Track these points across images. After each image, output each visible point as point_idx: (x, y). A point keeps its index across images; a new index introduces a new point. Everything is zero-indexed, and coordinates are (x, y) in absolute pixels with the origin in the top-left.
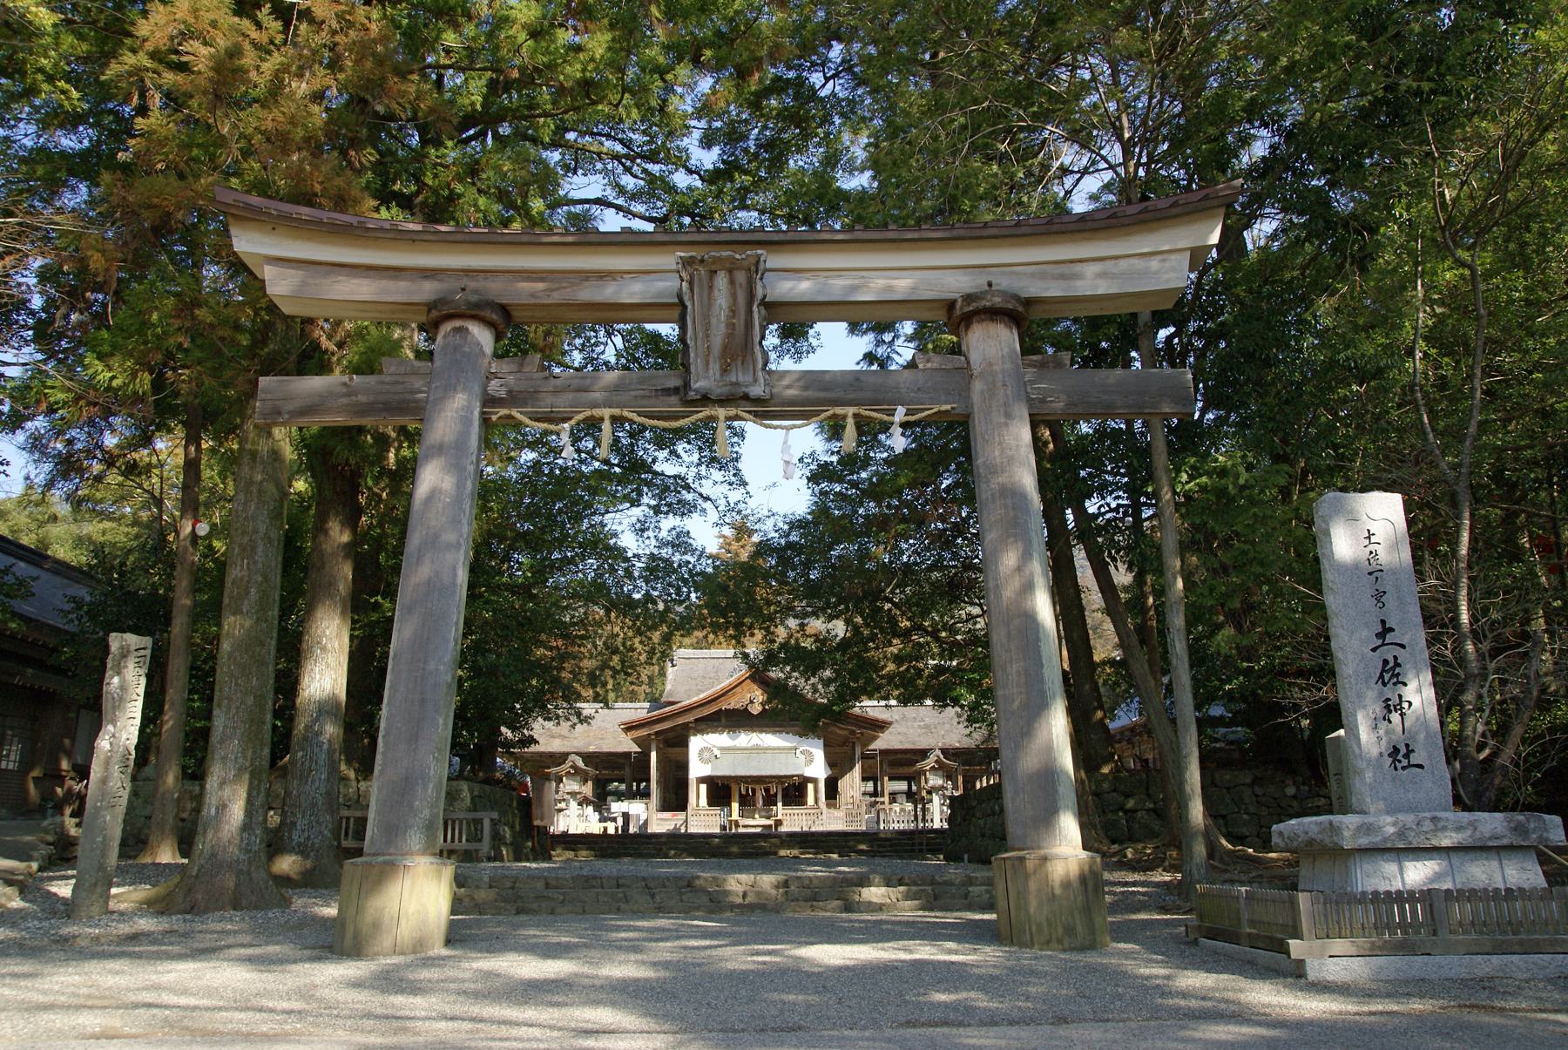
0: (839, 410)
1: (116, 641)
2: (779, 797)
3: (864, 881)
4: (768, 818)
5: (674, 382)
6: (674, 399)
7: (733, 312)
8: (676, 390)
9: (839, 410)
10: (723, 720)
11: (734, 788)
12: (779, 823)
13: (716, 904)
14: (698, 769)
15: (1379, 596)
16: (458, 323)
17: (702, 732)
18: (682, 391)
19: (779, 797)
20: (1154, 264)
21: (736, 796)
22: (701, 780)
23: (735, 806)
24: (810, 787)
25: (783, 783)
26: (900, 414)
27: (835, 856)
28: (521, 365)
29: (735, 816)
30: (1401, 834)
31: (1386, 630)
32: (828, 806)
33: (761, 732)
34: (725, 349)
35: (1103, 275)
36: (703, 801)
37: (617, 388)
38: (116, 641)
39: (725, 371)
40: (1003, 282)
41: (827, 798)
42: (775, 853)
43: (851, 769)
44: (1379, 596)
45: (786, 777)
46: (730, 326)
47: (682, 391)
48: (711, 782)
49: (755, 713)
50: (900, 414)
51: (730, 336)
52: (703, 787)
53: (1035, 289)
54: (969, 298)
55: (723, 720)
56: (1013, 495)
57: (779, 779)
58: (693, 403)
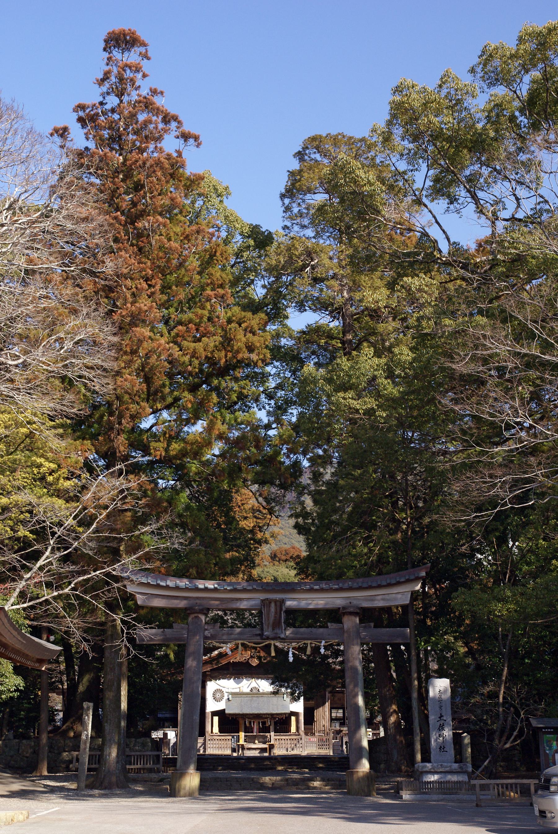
0: (306, 642)
1: (85, 705)
2: (272, 728)
3: (312, 779)
4: (264, 743)
5: (258, 632)
6: (259, 637)
7: (276, 613)
8: (259, 635)
9: (306, 642)
10: (231, 669)
11: (241, 722)
12: (272, 747)
13: (262, 787)
14: (212, 706)
15: (441, 707)
16: (196, 615)
17: (216, 678)
18: (261, 635)
19: (272, 728)
20: (399, 596)
21: (242, 727)
22: (214, 714)
23: (242, 735)
24: (293, 718)
25: (275, 718)
26: (323, 643)
27: (307, 770)
28: (214, 626)
29: (242, 742)
30: (433, 768)
31: (441, 716)
32: (306, 734)
33: (258, 678)
34: (274, 623)
35: (383, 599)
36: (216, 729)
37: (240, 633)
38: (85, 705)
39: (273, 629)
40: (355, 602)
41: (305, 724)
42: (275, 768)
43: (324, 704)
44: (441, 707)
45: (277, 714)
46: (275, 617)
47: (261, 635)
48: (220, 714)
49: (254, 665)
50: (323, 643)
51: (275, 620)
52: (216, 719)
53: (365, 605)
54: (344, 608)
55: (231, 669)
56: (355, 669)
57: (272, 716)
58: (265, 639)
